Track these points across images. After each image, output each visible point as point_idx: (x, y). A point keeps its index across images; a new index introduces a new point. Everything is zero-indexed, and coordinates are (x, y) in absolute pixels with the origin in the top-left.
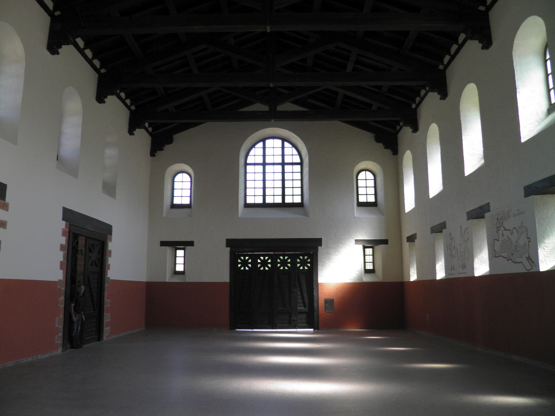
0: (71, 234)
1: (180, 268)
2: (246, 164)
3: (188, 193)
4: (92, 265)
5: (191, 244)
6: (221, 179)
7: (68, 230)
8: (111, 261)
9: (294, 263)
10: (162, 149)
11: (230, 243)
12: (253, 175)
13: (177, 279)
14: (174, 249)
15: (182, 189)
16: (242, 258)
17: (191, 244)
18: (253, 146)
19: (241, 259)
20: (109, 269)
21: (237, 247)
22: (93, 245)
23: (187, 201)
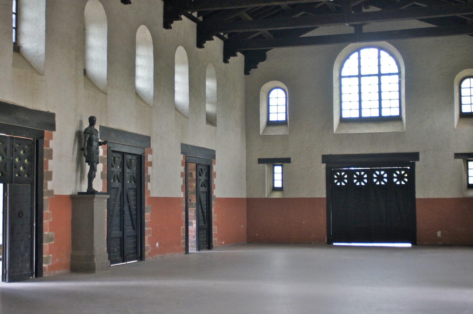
0: (192, 166)
1: (278, 184)
2: (399, 74)
3: (283, 109)
4: (202, 186)
5: (288, 160)
6: (314, 98)
7: (185, 161)
8: (216, 181)
9: (390, 178)
10: (256, 67)
11: (326, 159)
12: (349, 88)
13: (277, 195)
14: (272, 165)
15: (277, 104)
16: (338, 174)
17: (288, 160)
18: (347, 57)
19: (337, 175)
20: (214, 188)
21: (332, 163)
22: (202, 170)
23: (282, 117)
